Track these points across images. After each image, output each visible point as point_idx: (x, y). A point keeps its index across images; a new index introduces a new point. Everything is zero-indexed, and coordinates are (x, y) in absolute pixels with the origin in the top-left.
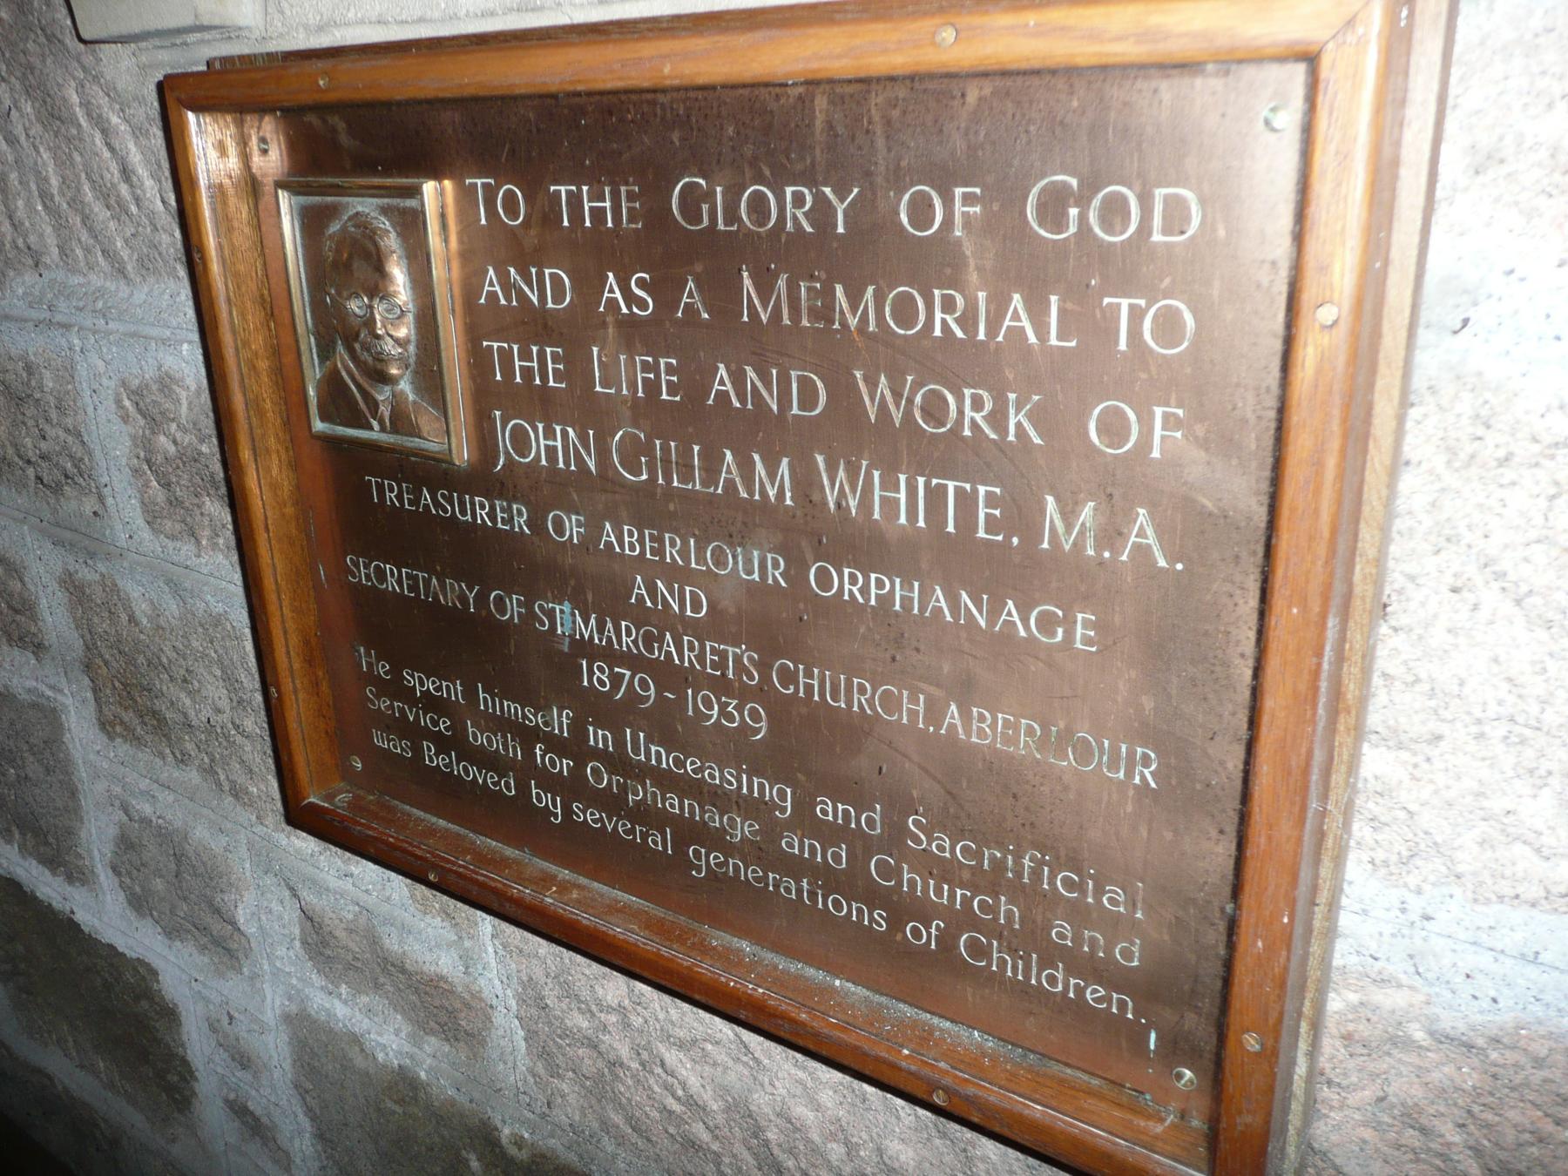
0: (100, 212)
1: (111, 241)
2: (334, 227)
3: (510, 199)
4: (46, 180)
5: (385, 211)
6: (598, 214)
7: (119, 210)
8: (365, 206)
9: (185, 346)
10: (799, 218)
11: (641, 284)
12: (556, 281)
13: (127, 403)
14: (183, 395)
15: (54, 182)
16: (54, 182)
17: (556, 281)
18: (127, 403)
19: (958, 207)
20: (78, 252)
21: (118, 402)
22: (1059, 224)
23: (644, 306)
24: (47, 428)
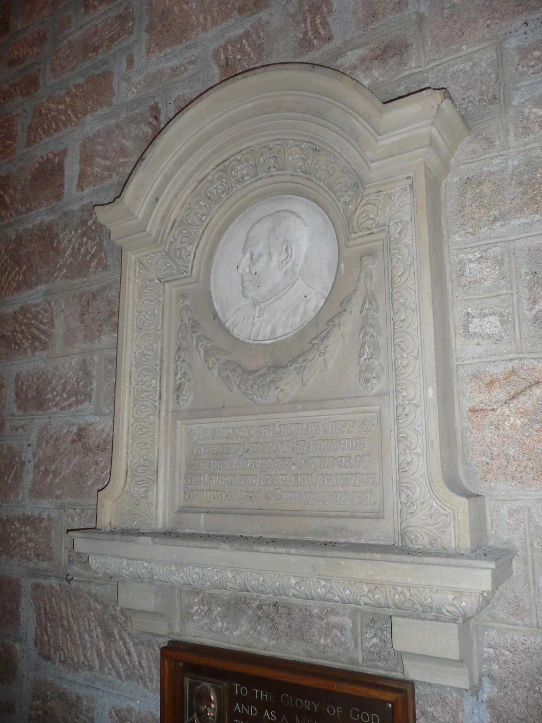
0: (117, 661)
1: (119, 669)
2: (198, 688)
3: (244, 690)
4: (100, 649)
5: (212, 687)
6: (264, 697)
7: (123, 661)
8: (208, 685)
9: (138, 701)
10: (308, 707)
11: (273, 713)
12: (253, 710)
13: (113, 713)
14: (133, 713)
15: (103, 649)
16: (103, 649)
17: (253, 710)
18: (113, 713)
19: (338, 711)
20: (106, 669)
21: (110, 713)
22: (356, 717)
23: (274, 718)
24: (80, 715)
